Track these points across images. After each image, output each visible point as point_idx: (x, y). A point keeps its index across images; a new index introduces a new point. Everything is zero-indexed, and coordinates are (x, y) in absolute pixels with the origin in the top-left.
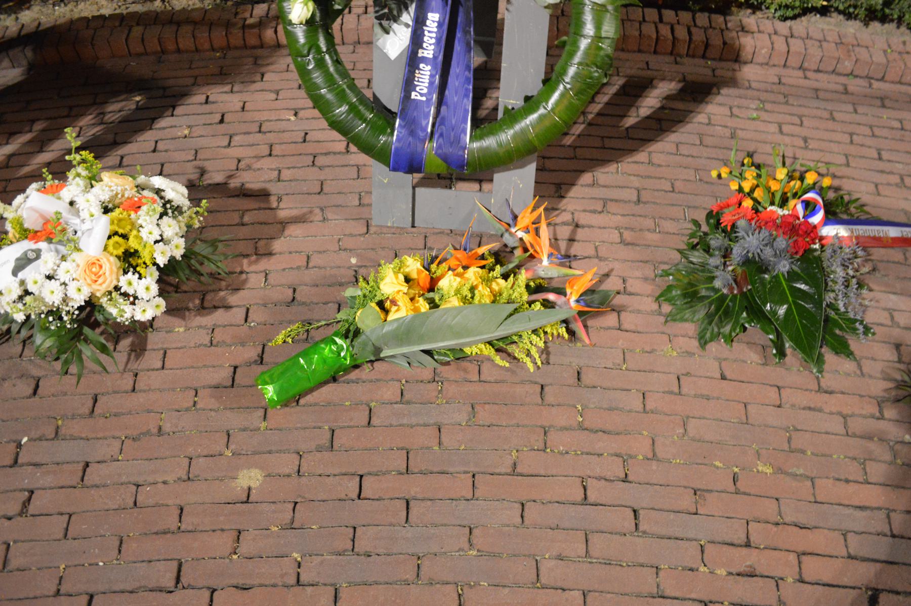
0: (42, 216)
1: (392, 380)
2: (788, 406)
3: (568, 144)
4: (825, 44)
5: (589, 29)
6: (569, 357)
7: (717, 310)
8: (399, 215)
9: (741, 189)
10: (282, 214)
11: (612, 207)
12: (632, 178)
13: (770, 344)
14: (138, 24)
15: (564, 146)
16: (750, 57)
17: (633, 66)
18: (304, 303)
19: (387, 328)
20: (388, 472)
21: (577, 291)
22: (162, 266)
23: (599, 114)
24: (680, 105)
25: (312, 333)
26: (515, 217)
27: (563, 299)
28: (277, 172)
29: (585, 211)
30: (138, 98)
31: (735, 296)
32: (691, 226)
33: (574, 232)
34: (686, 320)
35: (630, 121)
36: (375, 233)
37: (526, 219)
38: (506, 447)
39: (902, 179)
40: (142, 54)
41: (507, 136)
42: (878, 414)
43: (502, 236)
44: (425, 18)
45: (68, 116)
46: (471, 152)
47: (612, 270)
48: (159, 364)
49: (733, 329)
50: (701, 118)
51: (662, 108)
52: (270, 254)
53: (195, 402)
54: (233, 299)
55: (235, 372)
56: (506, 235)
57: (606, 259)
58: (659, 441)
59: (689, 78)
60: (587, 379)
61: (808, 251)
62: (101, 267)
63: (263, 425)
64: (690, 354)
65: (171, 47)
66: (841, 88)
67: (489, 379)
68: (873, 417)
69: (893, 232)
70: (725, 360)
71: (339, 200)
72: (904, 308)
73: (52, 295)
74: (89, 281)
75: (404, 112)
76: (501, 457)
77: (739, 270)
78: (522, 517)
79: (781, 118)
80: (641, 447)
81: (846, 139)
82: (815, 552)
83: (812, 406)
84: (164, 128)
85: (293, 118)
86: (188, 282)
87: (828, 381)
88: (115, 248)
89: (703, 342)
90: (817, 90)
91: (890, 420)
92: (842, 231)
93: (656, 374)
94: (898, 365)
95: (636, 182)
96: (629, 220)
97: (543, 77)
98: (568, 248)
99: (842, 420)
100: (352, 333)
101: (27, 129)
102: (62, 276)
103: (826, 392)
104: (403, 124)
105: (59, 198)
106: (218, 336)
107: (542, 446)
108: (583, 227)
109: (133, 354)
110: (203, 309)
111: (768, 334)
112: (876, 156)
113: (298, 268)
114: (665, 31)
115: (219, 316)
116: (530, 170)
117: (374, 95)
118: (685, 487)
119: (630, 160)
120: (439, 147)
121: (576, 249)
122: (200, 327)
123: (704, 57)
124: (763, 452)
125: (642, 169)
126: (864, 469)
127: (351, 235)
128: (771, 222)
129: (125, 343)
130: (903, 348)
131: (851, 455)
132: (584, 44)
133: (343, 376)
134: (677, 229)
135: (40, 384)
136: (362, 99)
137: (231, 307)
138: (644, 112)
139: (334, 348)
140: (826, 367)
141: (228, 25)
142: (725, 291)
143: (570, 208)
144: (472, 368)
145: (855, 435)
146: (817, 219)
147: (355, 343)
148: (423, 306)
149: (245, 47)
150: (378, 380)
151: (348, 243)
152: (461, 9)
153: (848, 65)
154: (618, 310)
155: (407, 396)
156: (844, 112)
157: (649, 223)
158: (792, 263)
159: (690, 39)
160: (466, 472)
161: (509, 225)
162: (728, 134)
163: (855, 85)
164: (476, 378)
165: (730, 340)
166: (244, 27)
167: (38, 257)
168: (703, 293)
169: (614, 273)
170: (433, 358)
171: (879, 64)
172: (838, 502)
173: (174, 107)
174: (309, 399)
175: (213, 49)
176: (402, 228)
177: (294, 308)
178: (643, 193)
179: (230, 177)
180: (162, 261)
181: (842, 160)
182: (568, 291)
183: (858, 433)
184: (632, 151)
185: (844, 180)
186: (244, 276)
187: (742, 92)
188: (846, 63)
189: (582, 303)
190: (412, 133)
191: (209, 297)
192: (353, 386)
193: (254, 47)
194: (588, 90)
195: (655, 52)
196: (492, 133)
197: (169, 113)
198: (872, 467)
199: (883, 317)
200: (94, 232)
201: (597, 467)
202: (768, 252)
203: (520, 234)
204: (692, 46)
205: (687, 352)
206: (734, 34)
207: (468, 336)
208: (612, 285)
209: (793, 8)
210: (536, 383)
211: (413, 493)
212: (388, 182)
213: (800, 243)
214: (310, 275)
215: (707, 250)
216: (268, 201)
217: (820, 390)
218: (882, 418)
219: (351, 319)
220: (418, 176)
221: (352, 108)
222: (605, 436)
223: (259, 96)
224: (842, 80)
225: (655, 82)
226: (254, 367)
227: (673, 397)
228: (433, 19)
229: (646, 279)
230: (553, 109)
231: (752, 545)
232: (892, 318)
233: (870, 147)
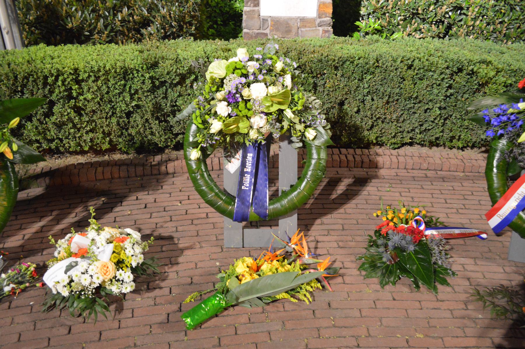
0: (79, 247)
1: (244, 313)
5: (315, 156)
6: (323, 298)
7: (386, 271)
9: (387, 219)
10: (181, 246)
11: (332, 233)
13: (412, 283)
14: (100, 166)
16: (382, 166)
17: (332, 173)
18: (197, 284)
19: (242, 288)
21: (323, 268)
22: (134, 267)
23: (319, 194)
25: (203, 296)
26: (290, 239)
28: (175, 228)
29: (320, 235)
30: (103, 199)
31: (393, 265)
32: (368, 237)
33: (316, 244)
34: (374, 277)
35: (333, 196)
37: (295, 239)
39: (458, 211)
40: (102, 180)
41: (285, 202)
42: (465, 308)
45: (69, 208)
46: (270, 210)
47: (336, 259)
48: (131, 315)
49: (395, 278)
50: (365, 193)
51: (347, 190)
52: (178, 264)
53: (151, 331)
54: (163, 284)
55: (168, 316)
56: (287, 247)
57: (333, 255)
58: (371, 329)
59: (357, 176)
60: (333, 305)
61: (420, 241)
62: (108, 268)
63: (186, 338)
65: (116, 175)
66: (424, 175)
67: (289, 310)
68: (463, 309)
69: (457, 231)
71: (207, 238)
73: (85, 281)
74: (103, 274)
75: (239, 195)
77: (393, 253)
79: (400, 190)
80: (363, 332)
81: (430, 196)
84: (118, 211)
85: (179, 204)
86: (142, 276)
87: (440, 296)
88: (114, 259)
89: (383, 285)
90: (414, 177)
91: (471, 310)
92: (434, 232)
93: (364, 301)
94: (470, 287)
95: (341, 221)
96: (342, 235)
97: (297, 177)
98: (315, 251)
99: (450, 312)
100: (226, 291)
101: (49, 214)
102: (90, 272)
103: (441, 301)
105: (87, 238)
106: (158, 300)
108: (320, 242)
109: (117, 312)
110: (149, 289)
112: (444, 202)
113: (192, 269)
114: (343, 157)
115: (157, 292)
116: (295, 216)
117: (224, 189)
120: (255, 209)
121: (319, 251)
122: (148, 298)
123: (362, 167)
124: (418, 329)
125: (343, 216)
126: (464, 331)
127: (215, 253)
128: (403, 230)
129: (113, 307)
130: (471, 279)
132: (313, 162)
133: (221, 314)
134: (362, 239)
135: (72, 328)
136: (220, 191)
137: (162, 288)
139: (218, 299)
140: (439, 291)
141: (143, 165)
142: (388, 263)
143: (313, 234)
145: (457, 318)
146: (422, 227)
148: (256, 276)
149: (152, 175)
150: (237, 314)
151: (214, 256)
152: (261, 151)
153: (425, 166)
154: (342, 276)
155: (252, 320)
156: (427, 185)
157: (349, 238)
159: (355, 160)
162: (378, 198)
163: (430, 174)
164: (282, 310)
165: (394, 283)
166: (151, 166)
167: (77, 265)
168: (379, 265)
171: (438, 164)
173: (121, 202)
174: (206, 325)
175: (136, 176)
177: (193, 286)
178: (345, 226)
179: (153, 231)
180: (134, 265)
181: (430, 205)
182: (319, 268)
184: (337, 209)
186: (166, 274)
187: (380, 180)
188: (424, 165)
190: (243, 203)
191: (151, 284)
192: (226, 318)
193: (156, 175)
194: (317, 180)
195: (340, 167)
196: (278, 201)
197: (120, 204)
198: (466, 330)
199: (460, 268)
200: (105, 253)
202: (403, 242)
203: (293, 246)
206: (373, 157)
207: (279, 288)
208: (337, 265)
209: (397, 144)
210: (310, 309)
212: (232, 227)
213: (417, 238)
214: (198, 271)
215: (378, 246)
216: (173, 241)
217: (438, 300)
218: (467, 309)
219: (224, 285)
220: (244, 223)
221: (216, 194)
222: (346, 329)
223: (162, 195)
225: (342, 179)
226: (178, 313)
227: (373, 310)
229: (352, 261)
230: (303, 189)
232: (464, 267)
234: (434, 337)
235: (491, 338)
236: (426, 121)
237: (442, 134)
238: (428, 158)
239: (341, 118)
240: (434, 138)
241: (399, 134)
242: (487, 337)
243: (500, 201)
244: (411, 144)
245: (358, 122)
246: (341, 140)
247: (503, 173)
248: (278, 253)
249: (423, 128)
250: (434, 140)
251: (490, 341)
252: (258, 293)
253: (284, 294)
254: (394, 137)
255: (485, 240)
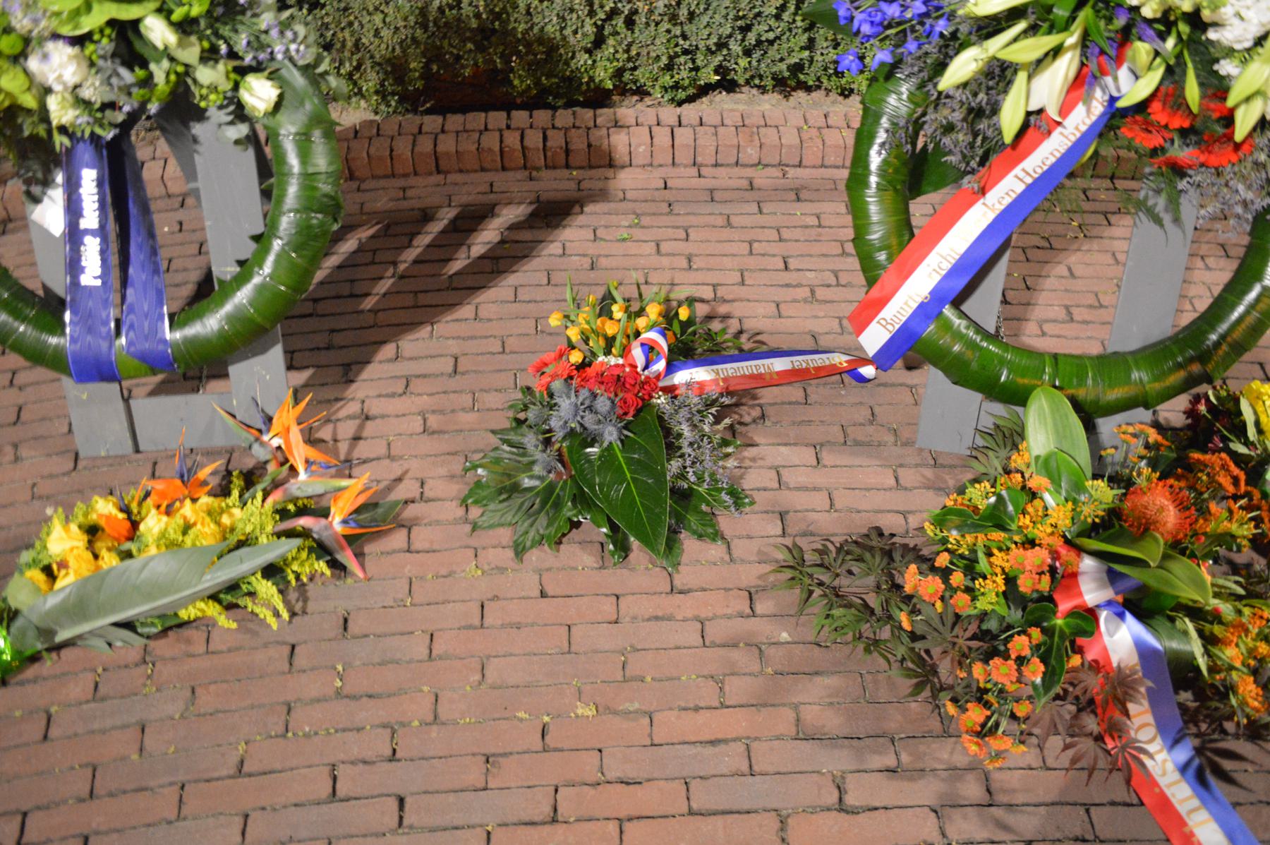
2: (627, 619)
3: (369, 307)
4: (721, 130)
8: (114, 436)
12: (450, 342)
15: (362, 311)
16: (627, 159)
20: (65, 802)
23: (416, 262)
24: (526, 235)
26: (270, 419)
27: (323, 522)
29: (380, 396)
35: (456, 266)
36: (85, 468)
38: (232, 739)
39: (813, 292)
43: (250, 447)
44: (79, 178)
46: (174, 345)
47: (406, 472)
50: (554, 248)
51: (502, 242)
56: (256, 447)
57: (401, 458)
59: (544, 197)
64: (502, 570)
66: (745, 183)
70: (549, 570)
72: (797, 463)
76: (223, 755)
78: (243, 834)
80: (418, 709)
82: (644, 814)
83: (660, 614)
89: (520, 551)
90: (712, 191)
92: (700, 374)
94: (780, 540)
96: (435, 397)
98: (352, 448)
104: (76, 319)
107: (281, 729)
108: (375, 418)
111: (599, 526)
112: (782, 266)
114: (512, 139)
116: (276, 354)
118: (474, 755)
119: (449, 318)
120: (130, 343)
123: (567, 166)
127: (51, 476)
131: (706, 673)
138: (477, 250)
143: (360, 395)
144: (197, 636)
147: (13, 630)
151: (44, 488)
153: (751, 153)
156: (745, 215)
158: (626, 427)
160: (171, 784)
161: (260, 431)
162: (587, 266)
163: (763, 178)
169: (409, 475)
170: (137, 633)
171: (790, 147)
172: (681, 740)
176: (122, 457)
183: (718, 642)
185: (736, 304)
187: (612, 205)
189: (353, 525)
192: (29, 688)
195: (504, 169)
201: (355, 746)
204: (549, 154)
205: (497, 568)
206: (604, 131)
207: (165, 595)
211: (94, 825)
222: (372, 702)
224: (749, 172)
225: (497, 209)
228: (89, 178)
231: (560, 819)
233: (774, 256)
234: (627, 713)
235: (796, 707)
236: (759, 14)
237: (807, 53)
238: (763, 130)
239: (498, 16)
240: (783, 66)
241: (682, 59)
242: (784, 705)
243: (886, 278)
244: (728, 85)
245: (549, 28)
246: (510, 83)
247: (896, 190)
248: (204, 473)
249: (751, 38)
250: (787, 74)
251: (791, 715)
252: (113, 610)
253: (201, 605)
254: (669, 68)
255: (868, 385)
